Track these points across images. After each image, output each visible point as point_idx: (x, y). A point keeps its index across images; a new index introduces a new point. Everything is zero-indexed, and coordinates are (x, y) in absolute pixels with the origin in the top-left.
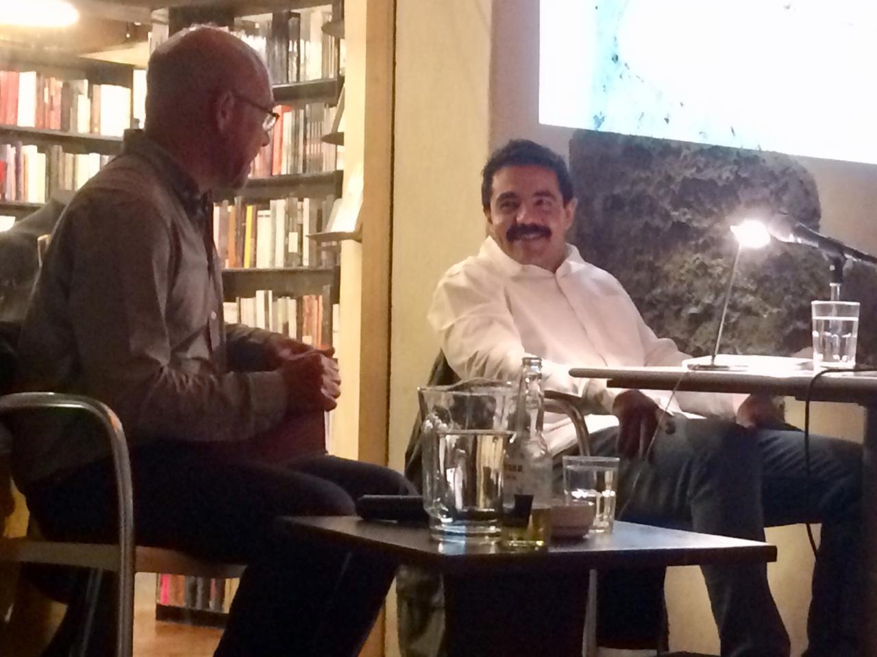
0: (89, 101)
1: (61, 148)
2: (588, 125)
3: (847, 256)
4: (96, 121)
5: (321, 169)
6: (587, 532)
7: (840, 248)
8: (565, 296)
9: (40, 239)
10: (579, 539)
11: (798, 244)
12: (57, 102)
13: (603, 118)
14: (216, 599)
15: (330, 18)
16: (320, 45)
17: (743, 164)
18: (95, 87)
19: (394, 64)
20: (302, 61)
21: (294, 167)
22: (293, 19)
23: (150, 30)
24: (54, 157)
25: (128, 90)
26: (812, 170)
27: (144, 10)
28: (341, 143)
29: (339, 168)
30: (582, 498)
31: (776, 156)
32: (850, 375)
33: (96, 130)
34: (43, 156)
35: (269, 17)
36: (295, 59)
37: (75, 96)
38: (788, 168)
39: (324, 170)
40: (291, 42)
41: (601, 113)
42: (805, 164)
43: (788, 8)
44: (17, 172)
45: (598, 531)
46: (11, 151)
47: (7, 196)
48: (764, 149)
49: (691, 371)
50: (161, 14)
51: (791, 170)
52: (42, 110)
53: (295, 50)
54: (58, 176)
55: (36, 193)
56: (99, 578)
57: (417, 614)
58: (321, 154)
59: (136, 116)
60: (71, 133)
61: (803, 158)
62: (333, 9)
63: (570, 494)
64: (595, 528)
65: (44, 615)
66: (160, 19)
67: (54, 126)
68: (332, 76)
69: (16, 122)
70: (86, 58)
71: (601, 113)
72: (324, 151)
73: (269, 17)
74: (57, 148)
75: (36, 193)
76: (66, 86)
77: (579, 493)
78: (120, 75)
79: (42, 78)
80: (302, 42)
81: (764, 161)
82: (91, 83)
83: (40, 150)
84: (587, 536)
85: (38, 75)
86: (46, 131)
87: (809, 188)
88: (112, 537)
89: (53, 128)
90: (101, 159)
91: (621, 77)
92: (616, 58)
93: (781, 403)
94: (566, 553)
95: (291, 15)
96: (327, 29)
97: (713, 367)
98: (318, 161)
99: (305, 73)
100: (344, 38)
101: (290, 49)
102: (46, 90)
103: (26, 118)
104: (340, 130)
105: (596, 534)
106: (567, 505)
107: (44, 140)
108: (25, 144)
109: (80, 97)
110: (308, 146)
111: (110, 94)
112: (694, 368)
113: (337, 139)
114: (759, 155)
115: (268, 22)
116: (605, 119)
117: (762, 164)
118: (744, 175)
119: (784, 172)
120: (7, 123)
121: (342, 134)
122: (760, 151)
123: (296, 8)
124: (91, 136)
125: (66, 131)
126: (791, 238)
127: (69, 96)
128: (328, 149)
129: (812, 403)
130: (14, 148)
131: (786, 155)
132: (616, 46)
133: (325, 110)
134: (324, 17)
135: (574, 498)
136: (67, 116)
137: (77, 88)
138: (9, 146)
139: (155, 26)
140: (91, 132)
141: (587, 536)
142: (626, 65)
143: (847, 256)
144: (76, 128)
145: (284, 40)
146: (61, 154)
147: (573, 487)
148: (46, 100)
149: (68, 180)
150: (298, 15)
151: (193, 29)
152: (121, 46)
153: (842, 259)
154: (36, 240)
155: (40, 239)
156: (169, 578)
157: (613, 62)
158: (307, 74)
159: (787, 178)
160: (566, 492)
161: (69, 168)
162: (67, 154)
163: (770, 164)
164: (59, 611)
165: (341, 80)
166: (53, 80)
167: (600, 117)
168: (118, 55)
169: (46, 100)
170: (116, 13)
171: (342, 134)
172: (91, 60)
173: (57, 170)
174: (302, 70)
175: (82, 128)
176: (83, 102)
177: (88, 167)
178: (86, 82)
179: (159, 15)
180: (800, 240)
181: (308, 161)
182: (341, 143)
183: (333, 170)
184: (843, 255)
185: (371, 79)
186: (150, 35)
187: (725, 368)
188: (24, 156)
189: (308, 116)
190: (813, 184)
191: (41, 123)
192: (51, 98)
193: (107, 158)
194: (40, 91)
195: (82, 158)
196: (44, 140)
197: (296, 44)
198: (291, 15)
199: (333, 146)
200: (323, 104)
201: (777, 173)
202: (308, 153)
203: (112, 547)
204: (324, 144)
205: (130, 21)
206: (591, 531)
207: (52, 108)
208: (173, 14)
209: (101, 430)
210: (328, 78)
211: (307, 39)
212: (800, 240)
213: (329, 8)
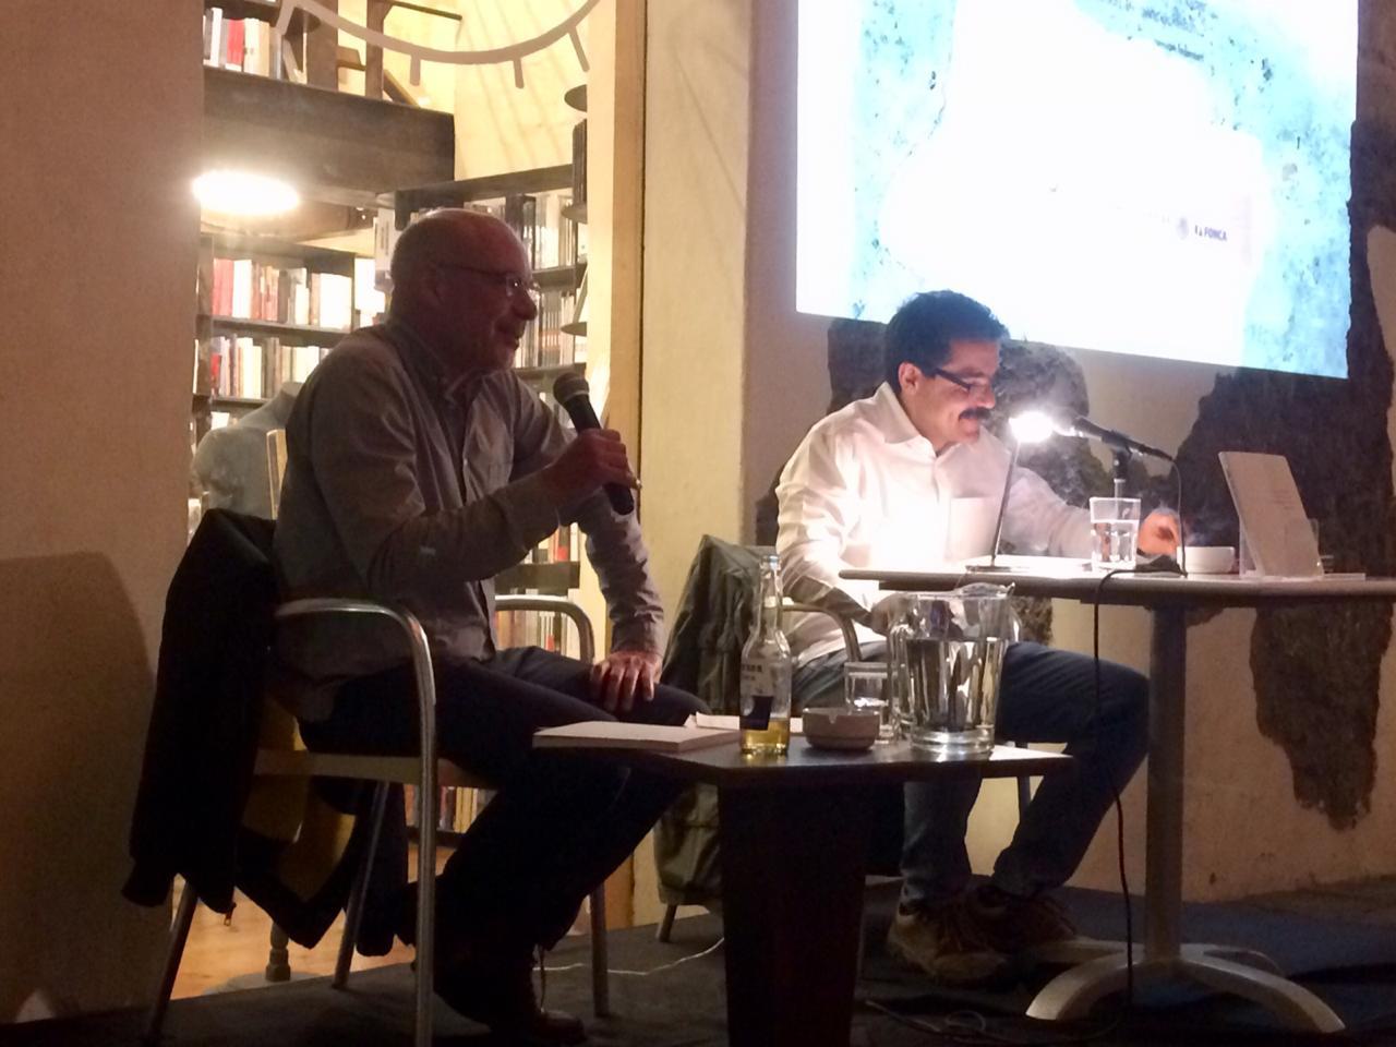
0: (307, 290)
1: (278, 341)
2: (849, 314)
3: (1132, 450)
4: (315, 312)
5: (558, 361)
6: (872, 743)
7: (1123, 441)
8: (937, 492)
9: (269, 434)
10: (864, 751)
11: (1080, 438)
12: (274, 292)
13: (863, 307)
14: (446, 819)
15: (570, 202)
16: (557, 231)
17: (1008, 355)
18: (314, 275)
19: (643, 248)
20: (537, 248)
21: (529, 360)
22: (528, 203)
23: (376, 216)
24: (270, 350)
25: (349, 280)
26: (1079, 362)
27: (370, 194)
28: (584, 334)
29: (579, 359)
30: (865, 707)
31: (1042, 348)
32: (1130, 576)
33: (315, 321)
34: (259, 350)
35: (502, 201)
36: (530, 246)
37: (292, 286)
38: (1053, 360)
39: (561, 363)
40: (525, 228)
41: (861, 301)
42: (1071, 355)
43: (1054, 190)
44: (232, 366)
45: (883, 742)
46: (225, 344)
47: (221, 391)
48: (1030, 339)
49: (970, 572)
50: (385, 198)
51: (1057, 363)
52: (258, 300)
53: (531, 236)
54: (274, 370)
55: (251, 389)
56: (387, 786)
57: (672, 833)
58: (558, 346)
59: (357, 307)
60: (288, 324)
61: (1070, 349)
62: (574, 192)
63: (853, 703)
64: (879, 738)
65: (334, 827)
66: (387, 204)
67: (271, 317)
68: (569, 263)
69: (231, 314)
70: (316, 248)
71: (861, 301)
72: (561, 343)
73: (502, 201)
74: (275, 340)
75: (251, 389)
76: (283, 274)
77: (861, 702)
78: (341, 264)
79: (258, 266)
80: (537, 228)
81: (1030, 352)
82: (309, 273)
83: (256, 343)
84: (872, 748)
85: (254, 263)
86: (261, 322)
87: (1077, 381)
88: (411, 748)
89: (269, 319)
90: (320, 352)
91: (881, 263)
92: (876, 243)
93: (1047, 607)
94: (858, 767)
95: (525, 199)
96: (566, 212)
97: (993, 568)
98: (556, 353)
99: (540, 260)
100: (585, 222)
101: (525, 236)
102: (262, 279)
103: (241, 310)
104: (581, 320)
105: (879, 745)
106: (850, 714)
107: (258, 332)
108: (240, 336)
109: (298, 286)
110: (544, 339)
111: (330, 285)
112: (973, 569)
113: (578, 329)
114: (1024, 346)
115: (501, 207)
116: (866, 307)
117: (1028, 356)
118: (1009, 367)
119: (1050, 364)
120: (221, 314)
121: (585, 324)
122: (1026, 342)
123: (532, 192)
124: (308, 327)
125: (283, 322)
126: (1072, 432)
127: (286, 285)
128: (565, 339)
129: (1101, 607)
130: (228, 341)
131: (1053, 346)
132: (877, 230)
133: (563, 300)
134: (560, 201)
135: (857, 707)
136: (284, 307)
137: (295, 278)
138: (223, 339)
139: (381, 211)
140: (310, 323)
141: (872, 748)
142: (887, 250)
143: (1132, 450)
144: (294, 320)
145: (518, 226)
146: (278, 347)
147: (857, 696)
148: (263, 290)
149: (285, 376)
150: (534, 199)
151: (431, 213)
152: (342, 233)
153: (1128, 454)
154: (265, 434)
155: (269, 434)
156: (483, 791)
157: (873, 248)
158: (543, 261)
159: (1052, 370)
160: (848, 701)
161: (286, 363)
162: (284, 347)
163: (1035, 353)
164: (348, 822)
165: (581, 269)
166: (270, 268)
167: (860, 305)
168: (338, 243)
169: (263, 290)
170: (337, 196)
171: (585, 324)
172: (306, 247)
173: (274, 361)
174: (537, 257)
175: (300, 319)
176: (301, 292)
177: (305, 363)
178: (304, 270)
179: (385, 199)
180: (1081, 434)
181: (544, 354)
182: (584, 334)
183: (571, 362)
184: (1127, 448)
185: (618, 264)
186: (375, 220)
187: (1006, 569)
188: (239, 349)
189: (543, 305)
190: (1079, 375)
191: (258, 314)
192: (268, 289)
193: (326, 351)
194: (256, 279)
195: (299, 351)
196: (258, 332)
197: (531, 230)
198: (525, 199)
199: (571, 337)
200: (560, 293)
201: (1043, 365)
202: (544, 345)
203: (413, 761)
204: (562, 334)
205: (351, 205)
206: (876, 742)
207: (268, 298)
208: (400, 196)
209: (406, 636)
210: (565, 265)
211: (543, 224)
212: (1081, 434)
213: (568, 192)
